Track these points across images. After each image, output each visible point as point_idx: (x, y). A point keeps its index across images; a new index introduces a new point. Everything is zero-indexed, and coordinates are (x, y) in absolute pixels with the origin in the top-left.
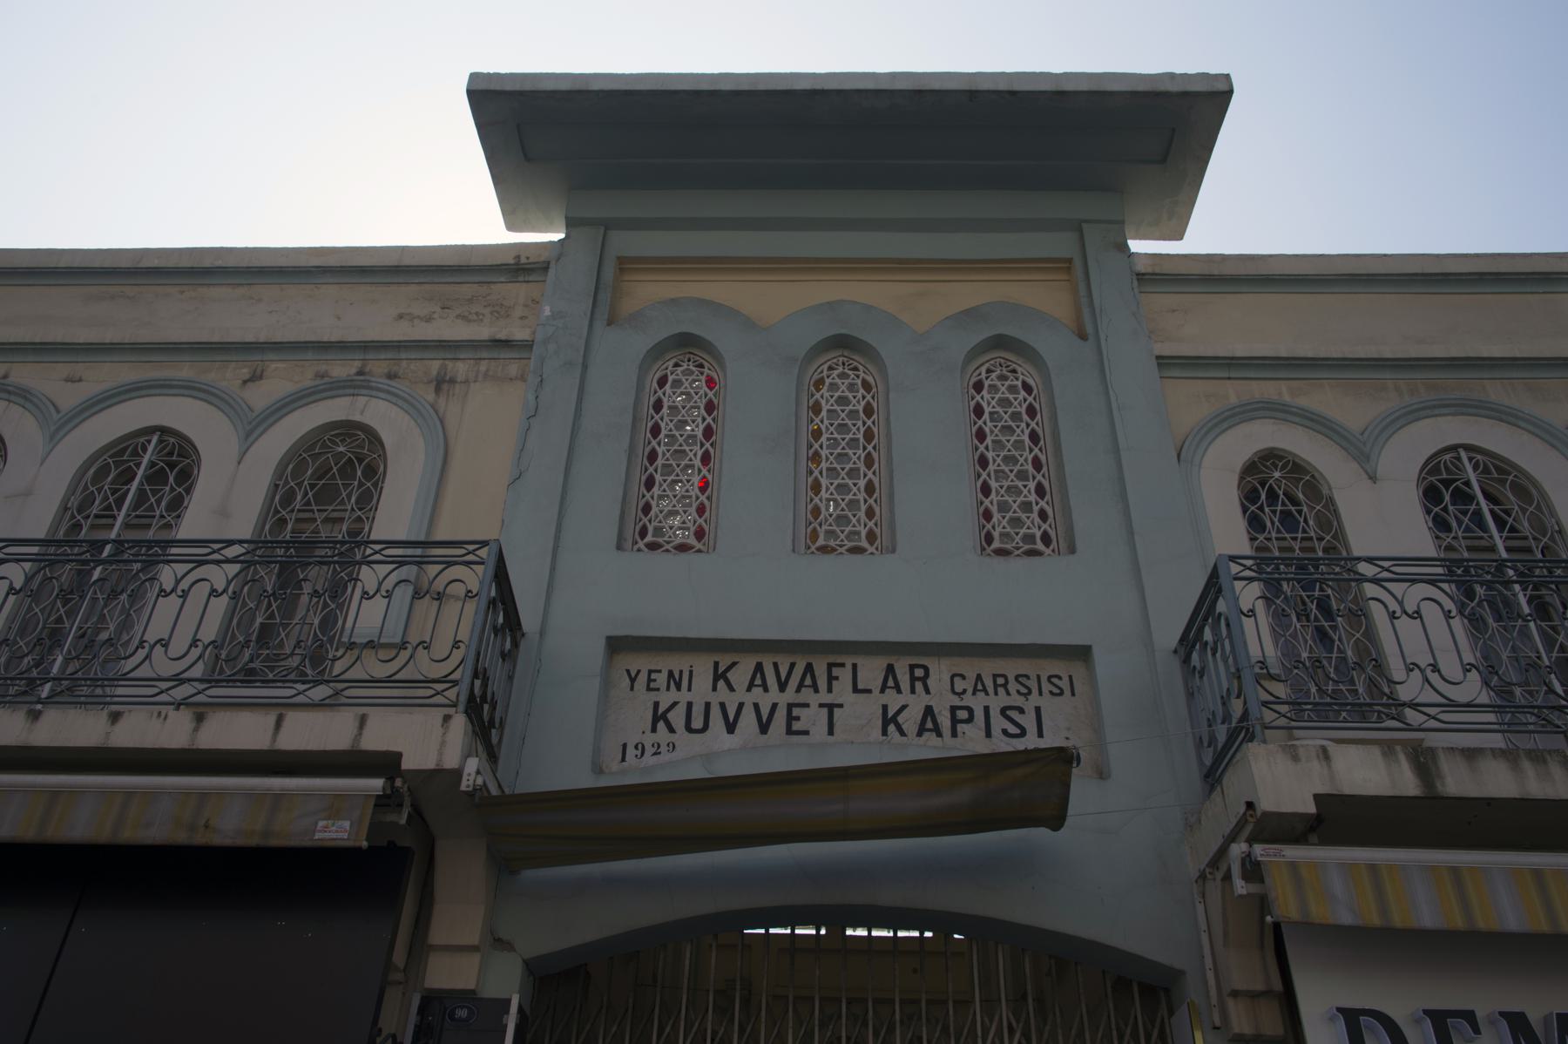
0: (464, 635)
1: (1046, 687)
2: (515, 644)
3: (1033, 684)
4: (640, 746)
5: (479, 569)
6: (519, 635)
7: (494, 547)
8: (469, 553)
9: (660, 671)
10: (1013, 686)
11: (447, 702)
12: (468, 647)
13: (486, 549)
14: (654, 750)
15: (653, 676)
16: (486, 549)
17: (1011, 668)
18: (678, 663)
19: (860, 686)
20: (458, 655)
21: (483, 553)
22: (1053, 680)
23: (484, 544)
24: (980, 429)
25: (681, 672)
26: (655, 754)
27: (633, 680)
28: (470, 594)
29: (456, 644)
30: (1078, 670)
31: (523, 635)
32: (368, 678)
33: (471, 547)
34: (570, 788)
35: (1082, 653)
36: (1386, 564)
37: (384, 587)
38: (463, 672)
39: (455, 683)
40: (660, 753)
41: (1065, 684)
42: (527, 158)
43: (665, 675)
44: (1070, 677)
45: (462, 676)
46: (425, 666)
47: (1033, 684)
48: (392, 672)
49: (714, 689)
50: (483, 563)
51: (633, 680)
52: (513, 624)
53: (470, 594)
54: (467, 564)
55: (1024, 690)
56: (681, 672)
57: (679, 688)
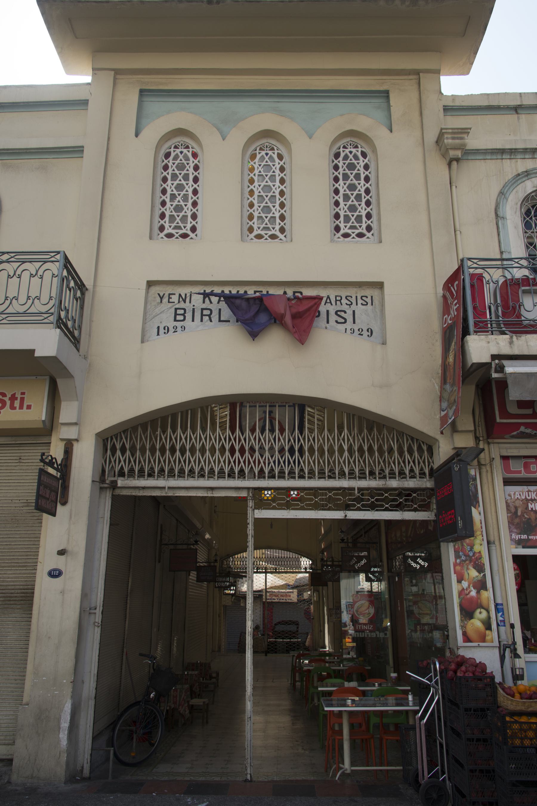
0: (54, 294)
1: (360, 301)
2: (83, 294)
3: (353, 300)
4: (166, 328)
5: (57, 264)
6: (84, 289)
7: (62, 254)
8: (52, 257)
9: (175, 294)
10: (344, 301)
11: (49, 322)
12: (55, 299)
13: (59, 255)
14: (174, 330)
15: (171, 296)
16: (59, 255)
17: (344, 292)
18: (184, 291)
19: (222, 319)
20: (52, 303)
21: (58, 257)
22: (363, 298)
23: (58, 253)
24: (251, 214)
25: (186, 295)
26: (174, 332)
27: (161, 298)
28: (54, 276)
29: (51, 298)
30: (376, 293)
31: (87, 289)
32: (16, 312)
33: (53, 254)
34: (70, 371)
35: (380, 285)
36: (475, 261)
37: (18, 273)
38: (55, 309)
39: (52, 314)
40: (177, 331)
41: (369, 300)
42: (76, 38)
43: (177, 295)
44: (372, 297)
45: (55, 311)
46: (38, 307)
47: (353, 300)
48: (26, 309)
49: (204, 302)
50: (58, 261)
51: (161, 298)
52: (81, 286)
53: (54, 276)
54: (52, 262)
55: (349, 303)
56: (186, 295)
57: (185, 302)
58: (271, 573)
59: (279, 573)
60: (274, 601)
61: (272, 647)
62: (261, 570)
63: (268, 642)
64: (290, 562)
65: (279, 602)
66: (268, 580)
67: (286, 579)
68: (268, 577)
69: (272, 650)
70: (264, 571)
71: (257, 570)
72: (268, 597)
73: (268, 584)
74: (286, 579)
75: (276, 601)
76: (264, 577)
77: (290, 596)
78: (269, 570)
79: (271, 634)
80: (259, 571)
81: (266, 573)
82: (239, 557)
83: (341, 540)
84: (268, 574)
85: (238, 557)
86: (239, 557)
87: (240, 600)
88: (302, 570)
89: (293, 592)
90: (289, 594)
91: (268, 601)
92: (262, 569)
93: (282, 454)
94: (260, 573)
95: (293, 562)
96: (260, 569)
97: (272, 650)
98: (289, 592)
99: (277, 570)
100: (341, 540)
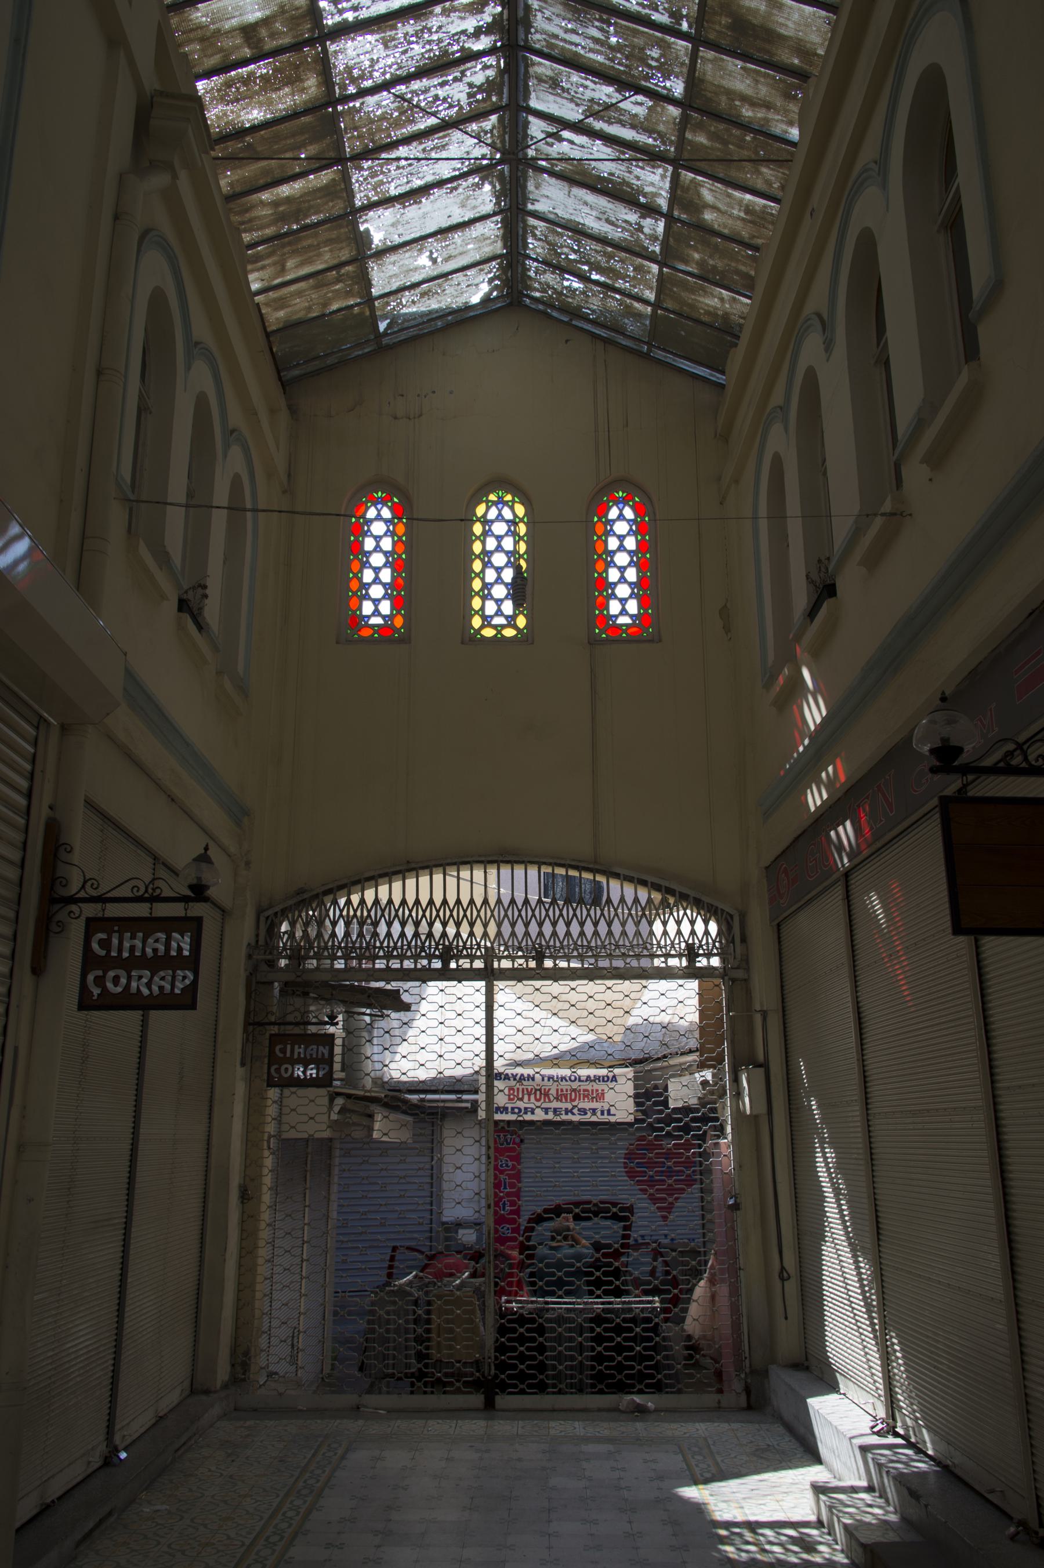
58: (517, 975)
59: (556, 975)
60: (528, 1117)
61: (522, 1358)
62: (465, 964)
63: (502, 1316)
64: (609, 924)
65: (547, 1123)
66: (499, 1030)
67: (592, 1021)
68: (500, 997)
69: (522, 1377)
70: (479, 964)
71: (446, 964)
72: (500, 1100)
73: (499, 1048)
74: (592, 1021)
75: (539, 1116)
76: (481, 998)
77: (600, 1096)
78: (506, 964)
79: (515, 1253)
80: (453, 965)
81: (489, 975)
82: (369, 902)
83: (191, 887)
84: (499, 984)
85: (362, 902)
86: (369, 902)
87: (371, 1116)
88: (673, 962)
89: (614, 1079)
90: (600, 1086)
91: (498, 1117)
92: (472, 958)
93: (475, 1077)
94: (461, 976)
95: (623, 924)
96: (458, 957)
97: (522, 1377)
98: (597, 1079)
99: (548, 963)
100: (191, 887)
